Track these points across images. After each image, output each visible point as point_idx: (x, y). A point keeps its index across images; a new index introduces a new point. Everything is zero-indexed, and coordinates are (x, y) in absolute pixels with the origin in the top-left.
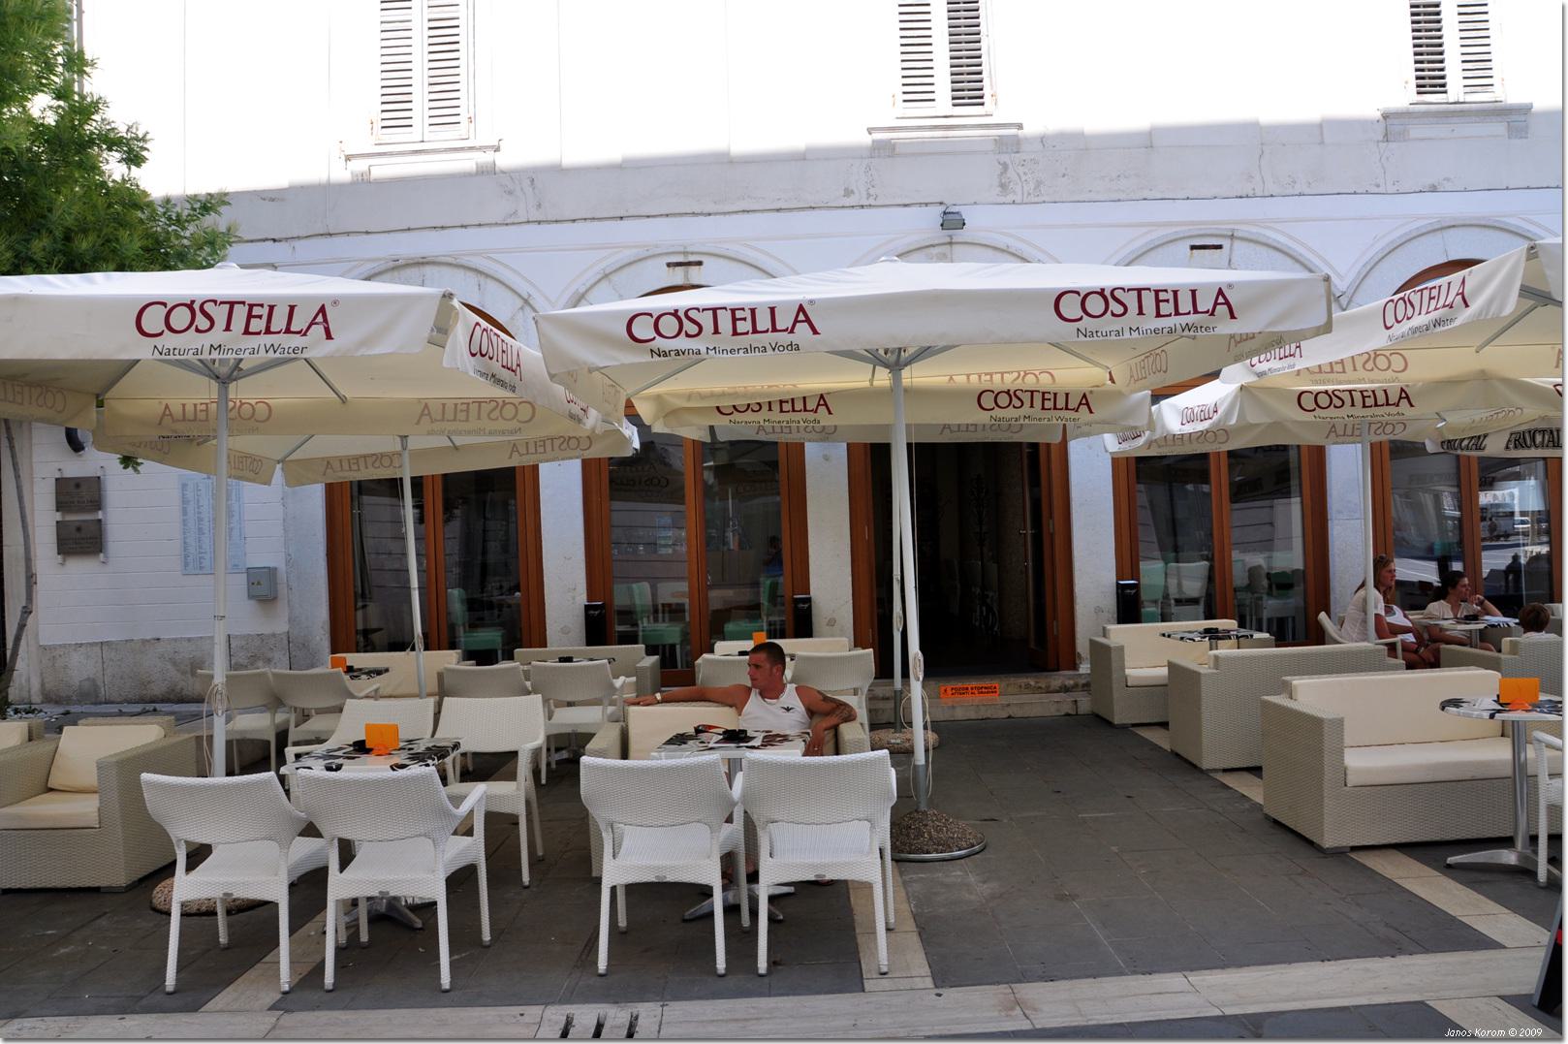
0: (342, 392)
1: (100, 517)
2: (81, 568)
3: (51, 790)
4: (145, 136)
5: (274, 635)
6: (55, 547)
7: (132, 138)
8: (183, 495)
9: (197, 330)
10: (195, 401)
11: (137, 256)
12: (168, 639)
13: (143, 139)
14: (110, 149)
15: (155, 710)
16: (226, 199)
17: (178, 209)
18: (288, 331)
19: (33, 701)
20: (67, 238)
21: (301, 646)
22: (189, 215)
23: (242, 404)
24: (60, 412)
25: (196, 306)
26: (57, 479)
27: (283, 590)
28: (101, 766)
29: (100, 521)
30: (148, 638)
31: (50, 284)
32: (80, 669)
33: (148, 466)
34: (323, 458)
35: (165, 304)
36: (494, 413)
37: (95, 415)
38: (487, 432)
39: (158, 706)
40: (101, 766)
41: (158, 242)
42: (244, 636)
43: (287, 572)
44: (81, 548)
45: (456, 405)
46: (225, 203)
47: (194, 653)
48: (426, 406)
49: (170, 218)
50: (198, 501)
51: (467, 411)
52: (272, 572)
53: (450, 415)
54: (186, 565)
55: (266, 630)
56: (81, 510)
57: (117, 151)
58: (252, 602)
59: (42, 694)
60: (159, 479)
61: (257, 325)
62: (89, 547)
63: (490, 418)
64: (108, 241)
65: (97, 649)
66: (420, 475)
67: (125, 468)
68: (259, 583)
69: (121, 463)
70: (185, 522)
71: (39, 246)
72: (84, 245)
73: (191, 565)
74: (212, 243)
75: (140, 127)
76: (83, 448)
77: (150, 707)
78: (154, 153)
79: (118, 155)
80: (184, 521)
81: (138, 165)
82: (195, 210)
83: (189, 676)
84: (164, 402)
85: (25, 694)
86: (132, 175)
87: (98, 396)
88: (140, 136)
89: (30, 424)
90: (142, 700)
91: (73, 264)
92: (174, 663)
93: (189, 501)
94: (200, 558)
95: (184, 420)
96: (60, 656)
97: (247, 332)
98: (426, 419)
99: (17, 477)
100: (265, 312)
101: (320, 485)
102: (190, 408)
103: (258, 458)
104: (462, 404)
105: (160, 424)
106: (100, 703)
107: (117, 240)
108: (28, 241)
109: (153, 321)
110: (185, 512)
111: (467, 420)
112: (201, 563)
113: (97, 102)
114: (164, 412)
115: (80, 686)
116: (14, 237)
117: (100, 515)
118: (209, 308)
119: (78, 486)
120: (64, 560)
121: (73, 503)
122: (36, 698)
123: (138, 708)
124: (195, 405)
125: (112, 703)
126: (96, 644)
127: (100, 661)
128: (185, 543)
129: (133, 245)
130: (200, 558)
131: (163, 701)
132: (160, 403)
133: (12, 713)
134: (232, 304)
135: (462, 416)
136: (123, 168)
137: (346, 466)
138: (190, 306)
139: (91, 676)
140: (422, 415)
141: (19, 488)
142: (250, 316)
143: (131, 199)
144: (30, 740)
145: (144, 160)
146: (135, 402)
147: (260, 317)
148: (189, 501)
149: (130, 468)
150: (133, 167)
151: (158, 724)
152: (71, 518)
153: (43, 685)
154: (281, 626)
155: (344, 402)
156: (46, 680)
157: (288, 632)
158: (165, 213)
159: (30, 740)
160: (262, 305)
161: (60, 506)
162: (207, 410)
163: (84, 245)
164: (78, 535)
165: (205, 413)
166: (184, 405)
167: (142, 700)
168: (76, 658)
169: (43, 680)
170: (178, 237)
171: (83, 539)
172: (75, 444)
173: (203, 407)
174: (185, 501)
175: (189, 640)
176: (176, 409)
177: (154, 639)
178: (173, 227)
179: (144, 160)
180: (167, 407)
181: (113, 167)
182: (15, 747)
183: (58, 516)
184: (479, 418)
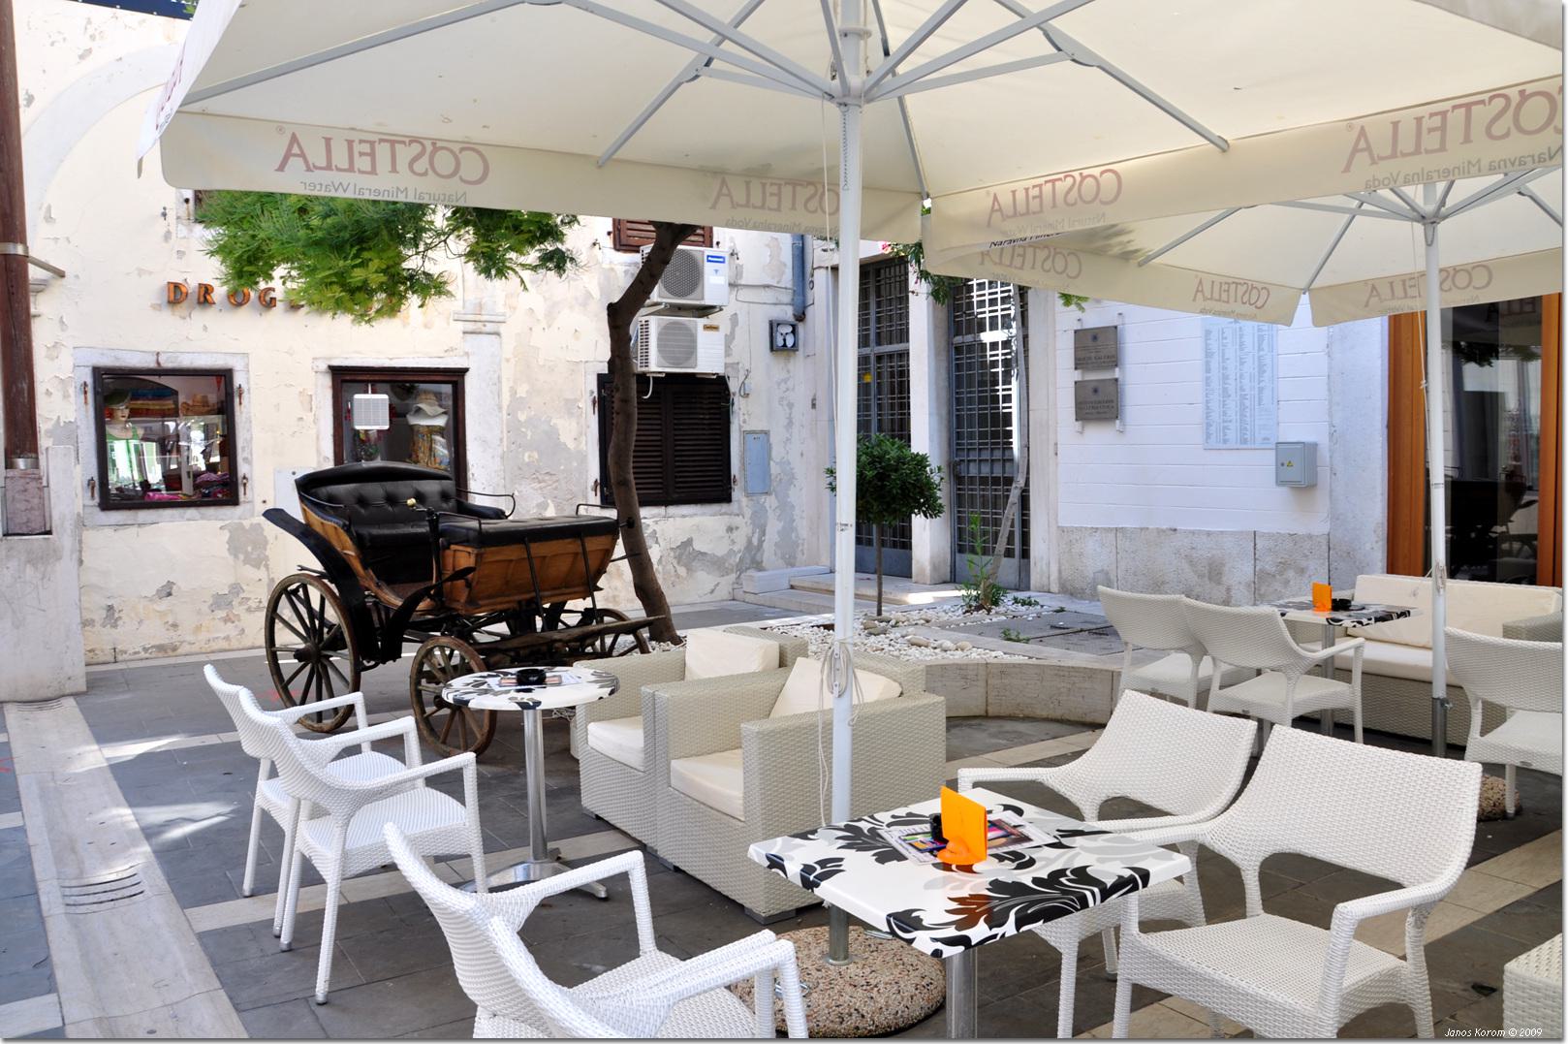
0: (1216, 131)
1: (1117, 376)
2: (1099, 435)
5: (1310, 537)
8: (1207, 344)
19: (1052, 590)
21: (1345, 555)
23: (1083, 178)
26: (1076, 332)
27: (1324, 474)
29: (1116, 380)
30: (1164, 527)
34: (1365, 282)
36: (1501, 122)
38: (1485, 163)
42: (1274, 535)
43: (1330, 450)
44: (1098, 413)
45: (1419, 120)
47: (1214, 552)
48: (1363, 132)
51: (1443, 128)
52: (1310, 450)
53: (1406, 143)
54: (1208, 436)
55: (1301, 530)
58: (1284, 490)
59: (1060, 584)
62: (1105, 413)
63: (1490, 136)
65: (1112, 536)
66: (1539, 295)
68: (1290, 465)
70: (1207, 381)
73: (1213, 437)
83: (1206, 579)
85: (1045, 581)
92: (1191, 563)
95: (1015, 214)
96: (1077, 540)
98: (1362, 158)
101: (1378, 320)
102: (1021, 196)
103: (1260, 286)
104: (1432, 115)
105: (989, 224)
111: (1443, 148)
112: (1225, 435)
114: (993, 208)
115: (1094, 579)
117: (1117, 373)
120: (1083, 427)
121: (1090, 358)
124: (1027, 190)
126: (1109, 530)
127: (1114, 551)
128: (1208, 408)
132: (988, 193)
135: (1431, 141)
137: (1399, 291)
139: (1105, 568)
140: (1355, 150)
153: (1060, 572)
154: (1319, 526)
155: (1224, 151)
157: (1328, 535)
159: (780, 666)
161: (1080, 363)
162: (1040, 196)
164: (1094, 398)
165: (1038, 200)
166: (1014, 192)
168: (1091, 546)
169: (1060, 567)
171: (1099, 402)
174: (1208, 354)
175: (1209, 534)
176: (1005, 200)
177: (1171, 530)
180: (995, 198)
182: (754, 673)
183: (1077, 376)
184: (1467, 139)
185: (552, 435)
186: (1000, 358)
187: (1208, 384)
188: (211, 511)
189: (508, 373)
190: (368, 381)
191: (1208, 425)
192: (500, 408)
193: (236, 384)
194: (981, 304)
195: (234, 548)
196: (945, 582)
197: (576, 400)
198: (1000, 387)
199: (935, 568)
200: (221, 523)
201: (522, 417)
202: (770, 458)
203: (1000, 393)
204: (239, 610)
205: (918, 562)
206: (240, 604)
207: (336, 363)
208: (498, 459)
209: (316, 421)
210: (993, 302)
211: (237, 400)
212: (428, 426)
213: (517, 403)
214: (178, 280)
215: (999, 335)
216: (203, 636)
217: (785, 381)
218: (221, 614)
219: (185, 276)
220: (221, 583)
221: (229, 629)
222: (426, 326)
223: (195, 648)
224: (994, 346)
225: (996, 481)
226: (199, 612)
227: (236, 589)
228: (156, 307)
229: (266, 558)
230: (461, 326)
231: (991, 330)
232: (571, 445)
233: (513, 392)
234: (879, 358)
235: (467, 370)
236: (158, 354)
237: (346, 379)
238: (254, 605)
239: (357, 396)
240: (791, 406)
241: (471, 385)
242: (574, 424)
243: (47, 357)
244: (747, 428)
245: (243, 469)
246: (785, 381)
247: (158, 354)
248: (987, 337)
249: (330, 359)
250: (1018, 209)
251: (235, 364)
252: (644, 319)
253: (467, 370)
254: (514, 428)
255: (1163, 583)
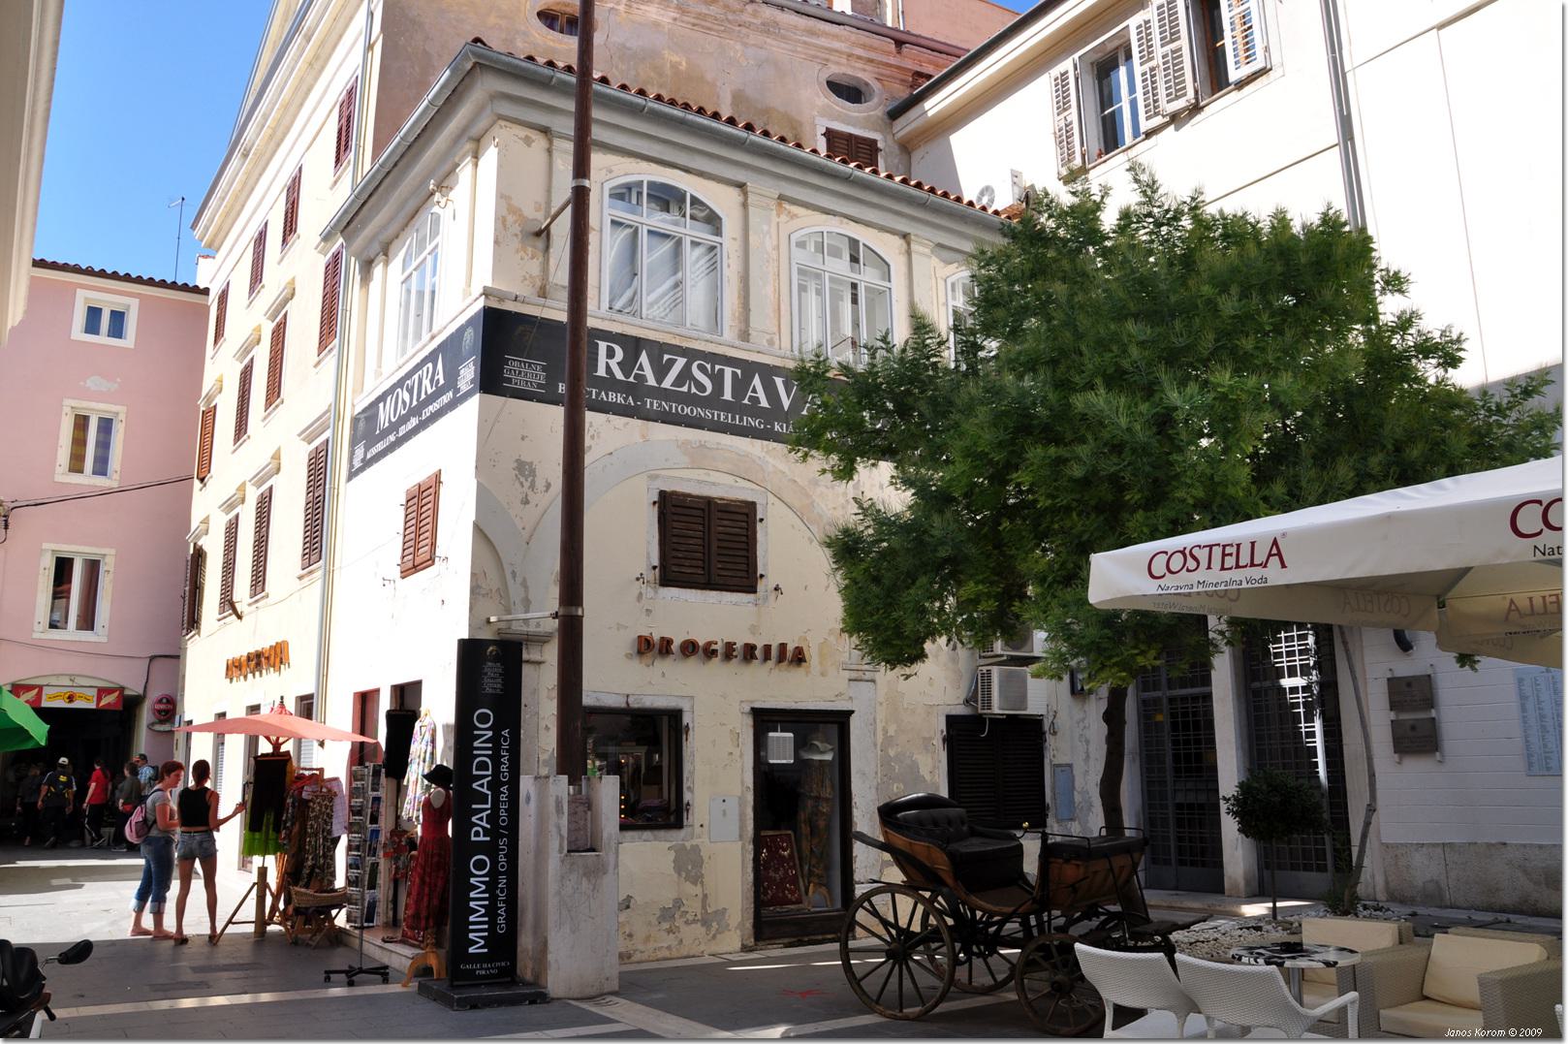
2: (1417, 768)
3: (1426, 998)
4: (1459, 338)
6: (1392, 747)
7: (1447, 343)
8: (1520, 690)
9: (1188, 570)
10: (1543, 593)
11: (1464, 454)
12: (1516, 845)
13: (1458, 340)
14: (1426, 357)
15: (1508, 921)
16: (1549, 378)
17: (1497, 399)
18: (1253, 565)
19: (1378, 898)
20: (1398, 449)
22: (1509, 402)
24: (1406, 616)
25: (1187, 552)
26: (1389, 679)
28: (1484, 982)
29: (1434, 719)
31: (1403, 497)
32: (1424, 870)
33: (1485, 662)
35: (1166, 553)
37: (1437, 617)
39: (1512, 917)
40: (1484, 982)
41: (1482, 436)
46: (1547, 383)
49: (1489, 410)
50: (1538, 696)
54: (1530, 765)
56: (1414, 709)
57: (1433, 357)
60: (1497, 672)
61: (1230, 562)
64: (1438, 444)
65: (1439, 850)
67: (1462, 666)
69: (1458, 662)
71: (1375, 462)
72: (1415, 453)
74: (1540, 427)
75: (1453, 330)
76: (1411, 648)
77: (1503, 917)
78: (1470, 354)
79: (1434, 361)
80: (1524, 717)
81: (1454, 367)
82: (1515, 396)
84: (1509, 597)
85: (1370, 890)
86: (1448, 375)
87: (1438, 597)
88: (1455, 337)
89: (1360, 629)
90: (1489, 908)
91: (1408, 476)
92: (1525, 872)
93: (1527, 697)
94: (1546, 758)
97: (1223, 568)
99: (1354, 679)
100: (1233, 550)
105: (1507, 619)
106: (1446, 907)
107: (1444, 441)
108: (1365, 459)
109: (1159, 567)
110: (1523, 709)
113: (1411, 317)
116: (1355, 457)
117: (1433, 713)
118: (1196, 551)
119: (1409, 685)
122: (1381, 896)
123: (1489, 917)
124: (1544, 597)
125: (1458, 908)
126: (1438, 844)
128: (1527, 741)
129: (1459, 443)
130: (1546, 758)
131: (1514, 912)
133: (1361, 909)
134: (1211, 547)
136: (1440, 372)
138: (1183, 552)
141: (1356, 689)
142: (1224, 555)
143: (1450, 400)
144: (1401, 943)
145: (1461, 360)
146: (1470, 602)
147: (1231, 555)
148: (1527, 697)
149: (1467, 667)
150: (1450, 369)
151: (1538, 942)
152: (1404, 716)
153: (1387, 883)
156: (1390, 879)
158: (1483, 407)
159: (1401, 943)
160: (1231, 545)
161: (1394, 706)
163: (1415, 452)
166: (1531, 599)
167: (1489, 908)
168: (1418, 859)
170: (1500, 426)
172: (1404, 644)
173: (1554, 599)
174: (1523, 697)
175: (1541, 847)
178: (1494, 418)
179: (1461, 360)
180: (1512, 602)
181: (1430, 371)
183: (1392, 716)
185: (914, 767)
186: (1301, 700)
187: (1525, 722)
188: (662, 833)
189: (881, 716)
190: (777, 722)
191: (1529, 756)
192: (875, 745)
193: (685, 723)
194: (1279, 655)
195: (679, 866)
196: (1255, 896)
197: (931, 739)
198: (1302, 725)
199: (1248, 882)
200: (668, 845)
201: (892, 753)
202: (1073, 788)
203: (1303, 730)
204: (679, 922)
205: (1230, 878)
206: (681, 916)
207: (757, 705)
208: (874, 790)
209: (741, 756)
210: (1290, 654)
211: (684, 737)
212: (820, 761)
213: (889, 740)
214: (645, 633)
215: (1299, 681)
216: (652, 945)
217: (1083, 720)
218: (666, 925)
219: (651, 630)
220: (667, 898)
221: (670, 940)
222: (822, 674)
223: (645, 957)
224: (1294, 690)
225: (1201, 806)
226: (650, 924)
227: (678, 903)
228: (629, 656)
229: (702, 876)
230: (847, 674)
231: (1289, 677)
232: (928, 777)
233: (885, 731)
234: (1171, 700)
235: (853, 712)
236: (628, 696)
237: (765, 720)
238: (691, 918)
239: (771, 734)
240: (1088, 742)
241: (855, 725)
242: (930, 760)
243: (548, 697)
244: (1056, 762)
245: (687, 797)
246: (1083, 720)
247: (628, 696)
248: (1287, 682)
249: (752, 702)
250: (1535, 608)
251: (685, 705)
252: (985, 669)
253: (853, 712)
254: (886, 762)
255: (1497, 890)
